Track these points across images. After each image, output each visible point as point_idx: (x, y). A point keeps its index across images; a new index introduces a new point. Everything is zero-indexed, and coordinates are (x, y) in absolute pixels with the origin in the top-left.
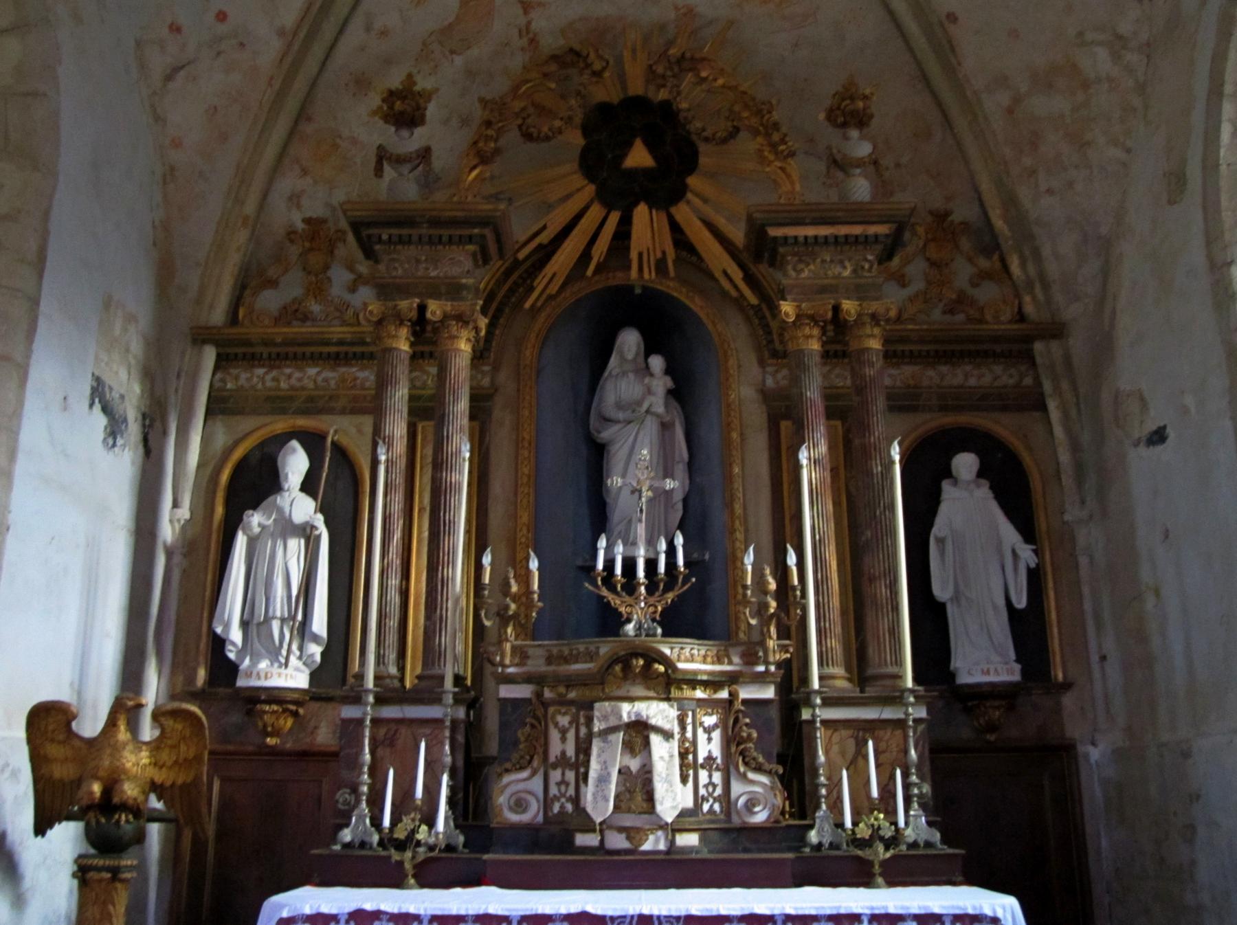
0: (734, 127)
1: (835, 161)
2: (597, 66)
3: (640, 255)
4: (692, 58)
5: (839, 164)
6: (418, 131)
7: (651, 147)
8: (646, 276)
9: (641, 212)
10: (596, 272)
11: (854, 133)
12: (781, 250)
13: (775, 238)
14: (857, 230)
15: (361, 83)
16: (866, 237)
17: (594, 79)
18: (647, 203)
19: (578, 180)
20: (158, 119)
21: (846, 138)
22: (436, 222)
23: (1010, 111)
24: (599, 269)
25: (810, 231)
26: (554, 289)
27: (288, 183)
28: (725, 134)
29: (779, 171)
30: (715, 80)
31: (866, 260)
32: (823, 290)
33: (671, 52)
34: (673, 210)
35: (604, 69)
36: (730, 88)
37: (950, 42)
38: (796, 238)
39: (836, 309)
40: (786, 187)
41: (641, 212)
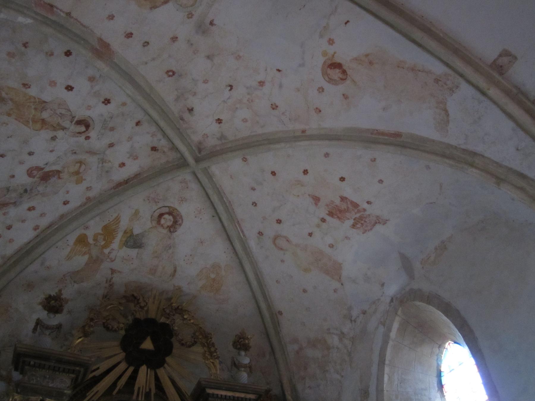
0: (195, 341)
1: (235, 364)
2: (142, 304)
3: (139, 388)
4: (182, 309)
5: (236, 365)
6: (58, 316)
7: (154, 341)
8: (140, 399)
9: (143, 369)
11: (243, 353)
13: (208, 394)
15: (30, 286)
16: (246, 399)
17: (140, 309)
18: (147, 365)
19: (118, 350)
21: (239, 354)
23: (297, 352)
24: (119, 392)
28: (191, 343)
29: (212, 364)
30: (190, 320)
34: (158, 371)
35: (145, 306)
36: (195, 325)
37: (278, 322)
38: (217, 395)
40: (213, 371)
41: (143, 369)
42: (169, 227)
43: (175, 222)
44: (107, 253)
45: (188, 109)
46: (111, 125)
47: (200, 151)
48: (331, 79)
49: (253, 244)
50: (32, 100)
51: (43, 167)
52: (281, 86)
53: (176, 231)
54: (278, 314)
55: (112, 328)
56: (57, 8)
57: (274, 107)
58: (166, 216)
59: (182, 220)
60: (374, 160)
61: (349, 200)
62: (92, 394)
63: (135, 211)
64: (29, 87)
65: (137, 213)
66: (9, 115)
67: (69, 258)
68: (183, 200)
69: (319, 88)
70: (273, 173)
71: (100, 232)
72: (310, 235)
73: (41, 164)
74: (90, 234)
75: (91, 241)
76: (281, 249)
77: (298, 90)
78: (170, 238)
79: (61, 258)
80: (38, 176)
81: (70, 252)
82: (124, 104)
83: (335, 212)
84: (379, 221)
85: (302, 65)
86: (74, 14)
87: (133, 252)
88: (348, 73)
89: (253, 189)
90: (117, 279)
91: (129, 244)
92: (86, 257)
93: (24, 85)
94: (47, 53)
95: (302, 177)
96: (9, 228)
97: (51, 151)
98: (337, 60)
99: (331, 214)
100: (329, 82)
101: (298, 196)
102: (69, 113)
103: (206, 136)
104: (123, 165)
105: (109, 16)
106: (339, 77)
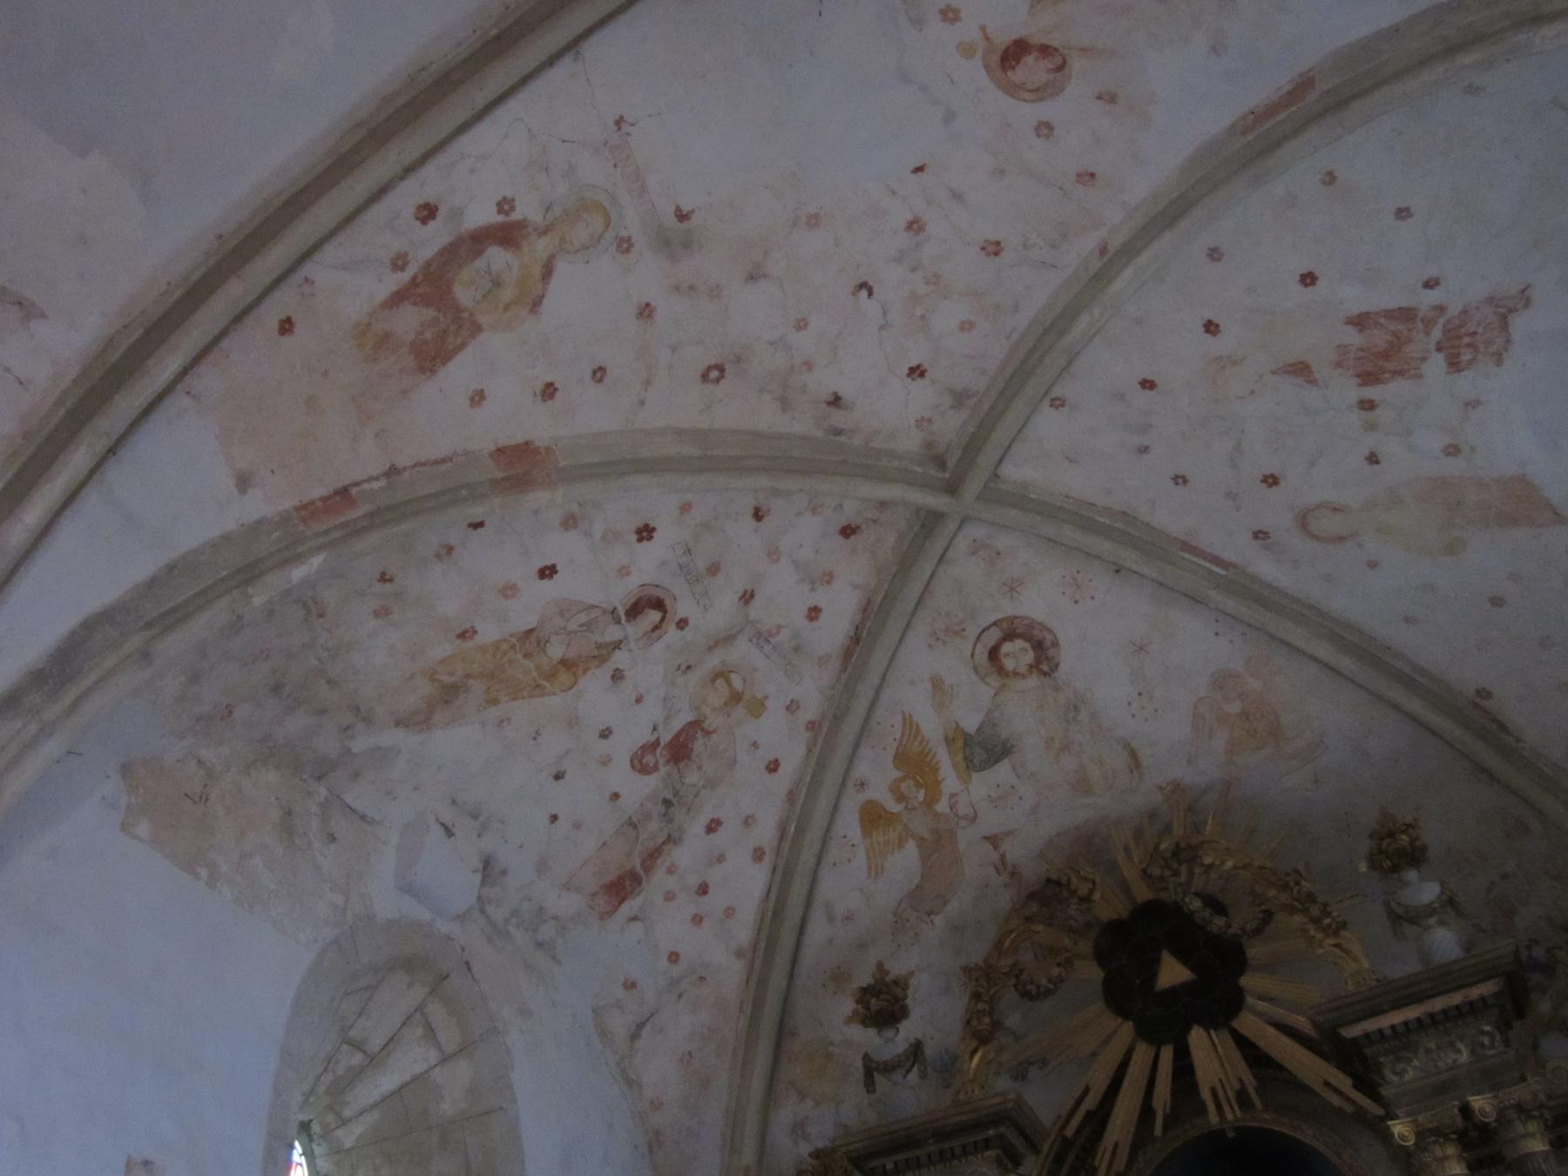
0: (1264, 912)
2: (1083, 890)
3: (1214, 1092)
5: (1404, 918)
7: (1183, 956)
8: (1230, 1117)
10: (1165, 1128)
11: (1411, 875)
12: (1368, 1051)
13: (1355, 1040)
14: (1456, 998)
18: (1199, 1024)
19: (1110, 1021)
20: (631, 1082)
22: (942, 1135)
24: (1171, 1121)
25: (1396, 1018)
26: (1120, 1165)
27: (785, 1114)
29: (1336, 950)
30: (1223, 862)
31: (1483, 1033)
32: (1441, 1089)
33: (1163, 846)
34: (1236, 1024)
35: (1091, 891)
38: (1380, 1031)
39: (1466, 1110)
42: (1034, 667)
43: (1038, 646)
44: (947, 810)
45: (829, 404)
46: (701, 565)
47: (941, 462)
48: (1038, 90)
49: (1265, 568)
50: (505, 646)
51: (653, 738)
52: (957, 197)
53: (1057, 665)
54: (1478, 700)
55: (1038, 987)
56: (357, 484)
57: (991, 249)
58: (1007, 647)
59: (1050, 631)
60: (1330, 178)
61: (1377, 313)
62: (1107, 1157)
63: (932, 684)
64: (475, 632)
65: (937, 684)
66: (495, 702)
67: (876, 870)
68: (1012, 588)
69: (1037, 128)
70: (1148, 384)
71: (897, 774)
72: (1373, 459)
73: (647, 737)
74: (879, 792)
75: (894, 807)
76: (1341, 539)
77: (1000, 172)
78: (1057, 689)
79: (861, 884)
80: (662, 761)
81: (868, 859)
82: (685, 508)
83: (1373, 369)
84: (1505, 308)
85: (950, 117)
86: (402, 461)
87: (1002, 771)
88: (1055, 44)
89: (1144, 450)
90: (1016, 851)
91: (977, 761)
92: (911, 846)
93: (462, 636)
94: (438, 556)
95: (1215, 345)
96: (703, 890)
97: (639, 700)
98: (1004, 39)
99: (1368, 378)
100: (1041, 99)
101: (1252, 392)
102: (595, 613)
103: (922, 422)
104: (814, 613)
105: (472, 400)
106: (1048, 71)
